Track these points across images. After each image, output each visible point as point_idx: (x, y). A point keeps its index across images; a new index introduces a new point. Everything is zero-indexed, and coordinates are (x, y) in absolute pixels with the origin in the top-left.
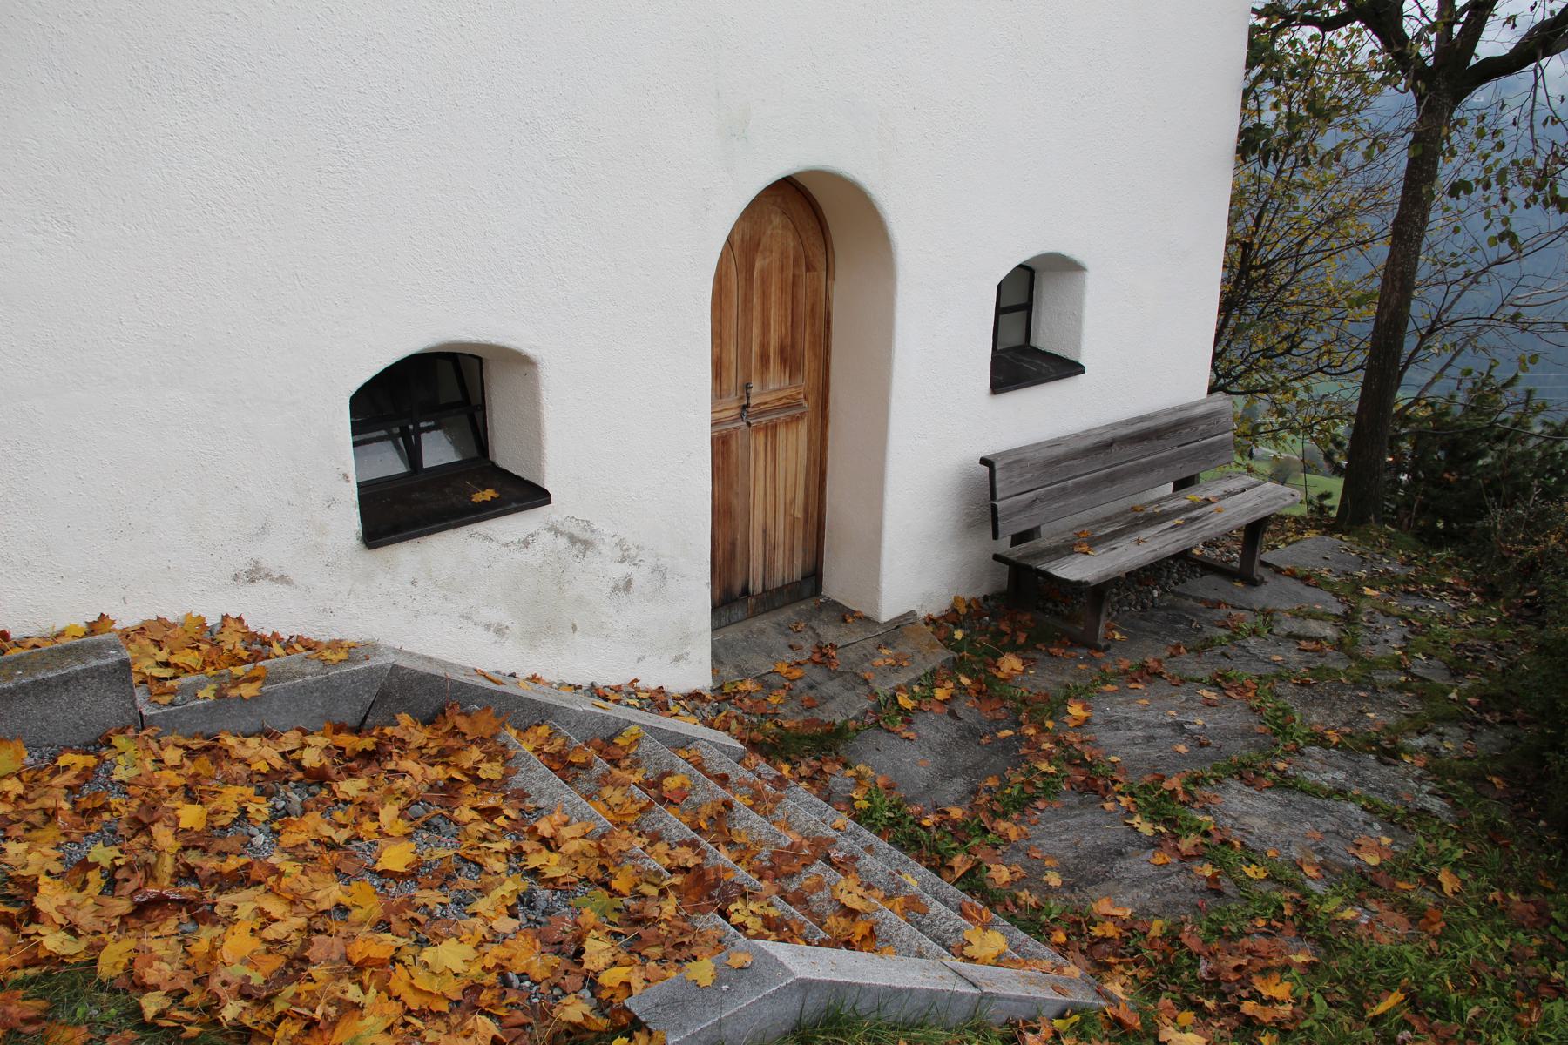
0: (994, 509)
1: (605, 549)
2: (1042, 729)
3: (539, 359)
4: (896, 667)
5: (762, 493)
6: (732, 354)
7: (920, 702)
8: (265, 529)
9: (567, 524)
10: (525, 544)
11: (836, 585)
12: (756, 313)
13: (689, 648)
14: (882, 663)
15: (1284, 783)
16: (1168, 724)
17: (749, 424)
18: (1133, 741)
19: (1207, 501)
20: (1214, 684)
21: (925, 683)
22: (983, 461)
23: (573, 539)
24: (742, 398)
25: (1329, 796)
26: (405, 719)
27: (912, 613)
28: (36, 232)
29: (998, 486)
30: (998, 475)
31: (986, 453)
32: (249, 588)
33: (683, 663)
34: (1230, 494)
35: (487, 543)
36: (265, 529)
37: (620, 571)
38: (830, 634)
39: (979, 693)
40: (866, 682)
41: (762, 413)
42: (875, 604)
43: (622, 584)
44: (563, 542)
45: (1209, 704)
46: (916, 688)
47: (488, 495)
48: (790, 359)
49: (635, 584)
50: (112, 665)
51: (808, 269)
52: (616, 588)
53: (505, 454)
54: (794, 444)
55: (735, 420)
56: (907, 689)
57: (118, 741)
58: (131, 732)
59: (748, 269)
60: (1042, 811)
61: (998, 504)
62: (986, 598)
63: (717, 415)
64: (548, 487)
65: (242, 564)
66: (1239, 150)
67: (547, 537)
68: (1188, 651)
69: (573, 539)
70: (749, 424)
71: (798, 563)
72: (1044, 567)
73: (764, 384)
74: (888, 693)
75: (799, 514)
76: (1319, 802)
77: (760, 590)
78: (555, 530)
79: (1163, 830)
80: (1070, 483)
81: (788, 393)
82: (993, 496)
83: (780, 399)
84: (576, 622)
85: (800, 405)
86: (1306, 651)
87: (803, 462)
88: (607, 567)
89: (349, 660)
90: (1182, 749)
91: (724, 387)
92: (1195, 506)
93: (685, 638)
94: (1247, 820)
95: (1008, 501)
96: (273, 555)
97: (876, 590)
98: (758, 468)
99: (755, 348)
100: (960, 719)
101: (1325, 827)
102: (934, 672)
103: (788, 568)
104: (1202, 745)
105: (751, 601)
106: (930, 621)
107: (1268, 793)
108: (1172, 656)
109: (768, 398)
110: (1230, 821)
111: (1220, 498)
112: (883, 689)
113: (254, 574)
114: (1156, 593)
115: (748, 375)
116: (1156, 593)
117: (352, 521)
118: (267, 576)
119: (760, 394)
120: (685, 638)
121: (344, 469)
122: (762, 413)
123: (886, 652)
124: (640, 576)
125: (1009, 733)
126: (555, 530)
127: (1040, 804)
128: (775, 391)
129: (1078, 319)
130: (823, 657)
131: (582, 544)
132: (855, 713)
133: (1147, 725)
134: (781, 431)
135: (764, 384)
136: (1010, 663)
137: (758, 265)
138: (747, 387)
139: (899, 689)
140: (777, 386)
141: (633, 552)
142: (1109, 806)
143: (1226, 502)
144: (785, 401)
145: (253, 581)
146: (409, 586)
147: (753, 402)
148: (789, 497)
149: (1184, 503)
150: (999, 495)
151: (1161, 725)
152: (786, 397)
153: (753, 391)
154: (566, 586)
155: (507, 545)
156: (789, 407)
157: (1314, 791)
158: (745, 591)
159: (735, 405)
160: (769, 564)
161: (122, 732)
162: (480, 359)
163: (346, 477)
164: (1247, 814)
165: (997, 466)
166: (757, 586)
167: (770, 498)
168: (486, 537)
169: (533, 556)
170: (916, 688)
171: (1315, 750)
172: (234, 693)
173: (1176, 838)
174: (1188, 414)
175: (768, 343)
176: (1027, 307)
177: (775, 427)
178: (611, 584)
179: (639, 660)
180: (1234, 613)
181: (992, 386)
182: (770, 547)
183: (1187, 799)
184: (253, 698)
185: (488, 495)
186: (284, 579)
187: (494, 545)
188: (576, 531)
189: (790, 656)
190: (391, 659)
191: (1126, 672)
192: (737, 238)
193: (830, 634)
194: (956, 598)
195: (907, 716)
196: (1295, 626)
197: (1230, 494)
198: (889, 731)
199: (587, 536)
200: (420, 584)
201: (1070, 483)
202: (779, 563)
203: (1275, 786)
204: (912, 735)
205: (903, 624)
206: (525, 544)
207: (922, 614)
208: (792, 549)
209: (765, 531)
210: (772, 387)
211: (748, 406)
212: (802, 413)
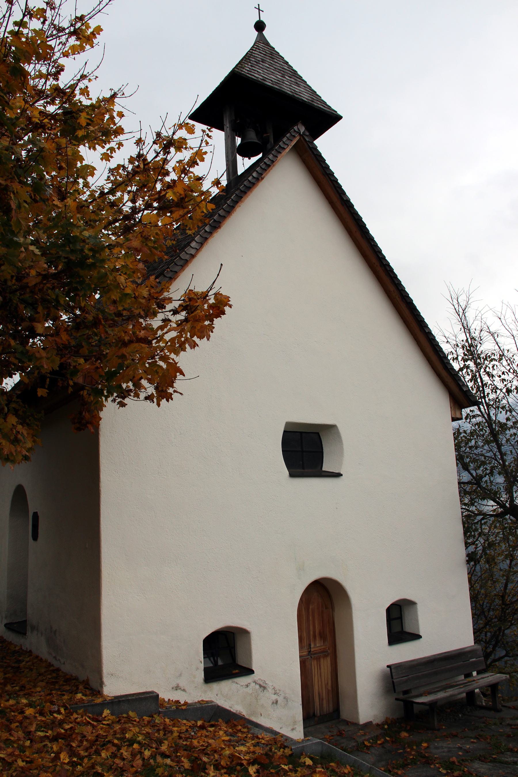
0: (393, 682)
1: (270, 690)
2: (412, 749)
3: (248, 629)
4: (365, 734)
5: (317, 680)
6: (305, 634)
7: (372, 744)
8: (180, 675)
9: (259, 681)
10: (247, 686)
11: (345, 714)
12: (311, 622)
13: (296, 726)
14: (360, 734)
15: (494, 761)
16: (457, 747)
17: (311, 657)
18: (444, 752)
19: (474, 680)
20: (476, 738)
21: (374, 739)
22: (388, 666)
23: (260, 686)
24: (308, 649)
25: (510, 764)
26: (220, 720)
27: (371, 722)
28: (138, 596)
29: (393, 674)
30: (393, 671)
31: (388, 664)
32: (175, 692)
33: (294, 731)
34: (483, 678)
35: (236, 685)
36: (180, 675)
37: (274, 697)
38: (342, 728)
39: (392, 742)
40: (354, 739)
41: (315, 654)
42: (357, 718)
43: (275, 702)
44: (257, 687)
45: (473, 742)
46: (371, 741)
47: (237, 671)
48: (323, 637)
49: (279, 702)
50: (154, 696)
51: (326, 609)
52: (273, 703)
53: (241, 661)
54: (326, 664)
55: (307, 656)
56: (368, 740)
57: (155, 716)
58: (157, 714)
59: (307, 609)
60: (410, 768)
61: (394, 680)
62: (398, 719)
63: (301, 654)
64: (253, 669)
65: (175, 685)
66: (467, 561)
67: (253, 684)
68: (469, 730)
69: (260, 686)
70: (311, 657)
71: (331, 706)
72: (412, 700)
73: (315, 644)
74: (361, 741)
75: (330, 688)
76: (507, 766)
77: (319, 714)
78: (255, 682)
79: (449, 771)
80: (420, 674)
81: (323, 647)
82: (392, 677)
83: (320, 649)
84: (262, 713)
85: (327, 651)
86: (513, 728)
87: (330, 670)
88: (269, 696)
89: (207, 703)
90: (460, 753)
91: (303, 645)
92: (469, 682)
93: (295, 723)
94: (479, 769)
95: (398, 680)
96: (183, 683)
97: (357, 712)
98: (315, 671)
99: (312, 633)
100: (385, 748)
101: (507, 771)
102: (377, 736)
103: (328, 707)
104: (467, 752)
105: (316, 719)
106: (378, 725)
107: (489, 764)
108: (462, 731)
109: (317, 649)
110: (473, 770)
111: (480, 679)
112: (360, 740)
113: (177, 688)
114: (460, 715)
115: (310, 642)
116: (460, 715)
117: (201, 675)
118: (180, 689)
119: (314, 647)
120: (295, 723)
121: (201, 660)
122: (315, 654)
123: (361, 731)
124: (280, 699)
125: (401, 751)
126: (255, 682)
127: (409, 766)
128: (319, 646)
129: (417, 620)
130: (340, 734)
131: (263, 687)
132: (350, 746)
133: (449, 748)
134: (322, 660)
135: (315, 644)
136: (404, 734)
137: (311, 607)
138: (310, 645)
139: (365, 740)
140: (319, 645)
141: (278, 691)
142: (432, 766)
143: (481, 680)
144: (322, 650)
145: (176, 690)
146: (216, 696)
147: (312, 650)
148: (326, 682)
149: (466, 681)
150: (394, 678)
151: (454, 748)
152: (323, 649)
153: (312, 646)
154: (259, 701)
155: (242, 686)
156: (323, 652)
157: (506, 763)
158: (314, 715)
159: (306, 651)
160: (321, 705)
161: (156, 714)
162: (233, 633)
163: (201, 662)
164: (14, 194)
165: (392, 667)
166: (318, 713)
167: (320, 683)
168: (237, 683)
169: (249, 690)
170: (371, 741)
171: (509, 753)
172: (180, 708)
173: (453, 772)
174: (463, 651)
175: (316, 631)
176: (400, 618)
177: (320, 658)
178: (272, 701)
179: (281, 728)
180: (488, 719)
181: (389, 642)
182: (321, 700)
183: (459, 764)
184: (185, 709)
185: (237, 671)
186: (184, 690)
187: (238, 685)
188: (261, 683)
189: (329, 734)
190: (215, 704)
191: (444, 736)
192: (304, 599)
193: (342, 728)
194: (387, 718)
195: (368, 748)
196: (511, 722)
197: (483, 678)
198: (362, 751)
199: (264, 685)
200: (219, 695)
201: (420, 674)
202: (325, 705)
203: (490, 762)
204: (369, 752)
205: (368, 725)
206: (247, 686)
207: (374, 723)
208: (329, 701)
209: (319, 694)
210: (318, 645)
211: (311, 651)
212: (328, 654)
